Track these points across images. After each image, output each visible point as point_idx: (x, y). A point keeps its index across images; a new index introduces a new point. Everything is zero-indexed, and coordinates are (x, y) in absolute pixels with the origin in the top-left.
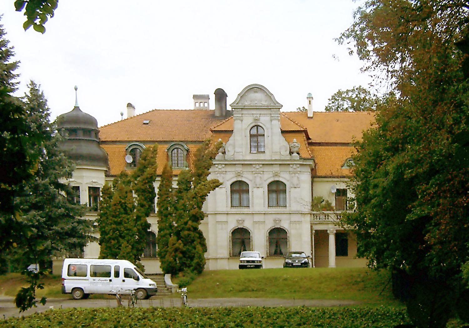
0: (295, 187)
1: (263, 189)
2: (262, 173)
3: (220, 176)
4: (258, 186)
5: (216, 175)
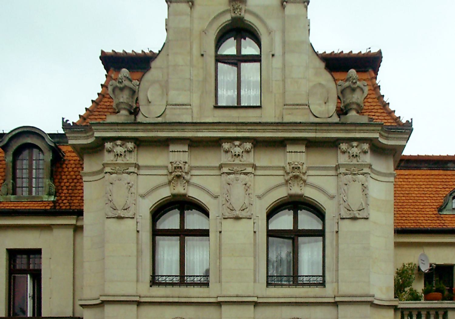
0: (120, 218)
1: (251, 222)
2: (249, 170)
3: (120, 180)
4: (238, 213)
5: (224, 177)
